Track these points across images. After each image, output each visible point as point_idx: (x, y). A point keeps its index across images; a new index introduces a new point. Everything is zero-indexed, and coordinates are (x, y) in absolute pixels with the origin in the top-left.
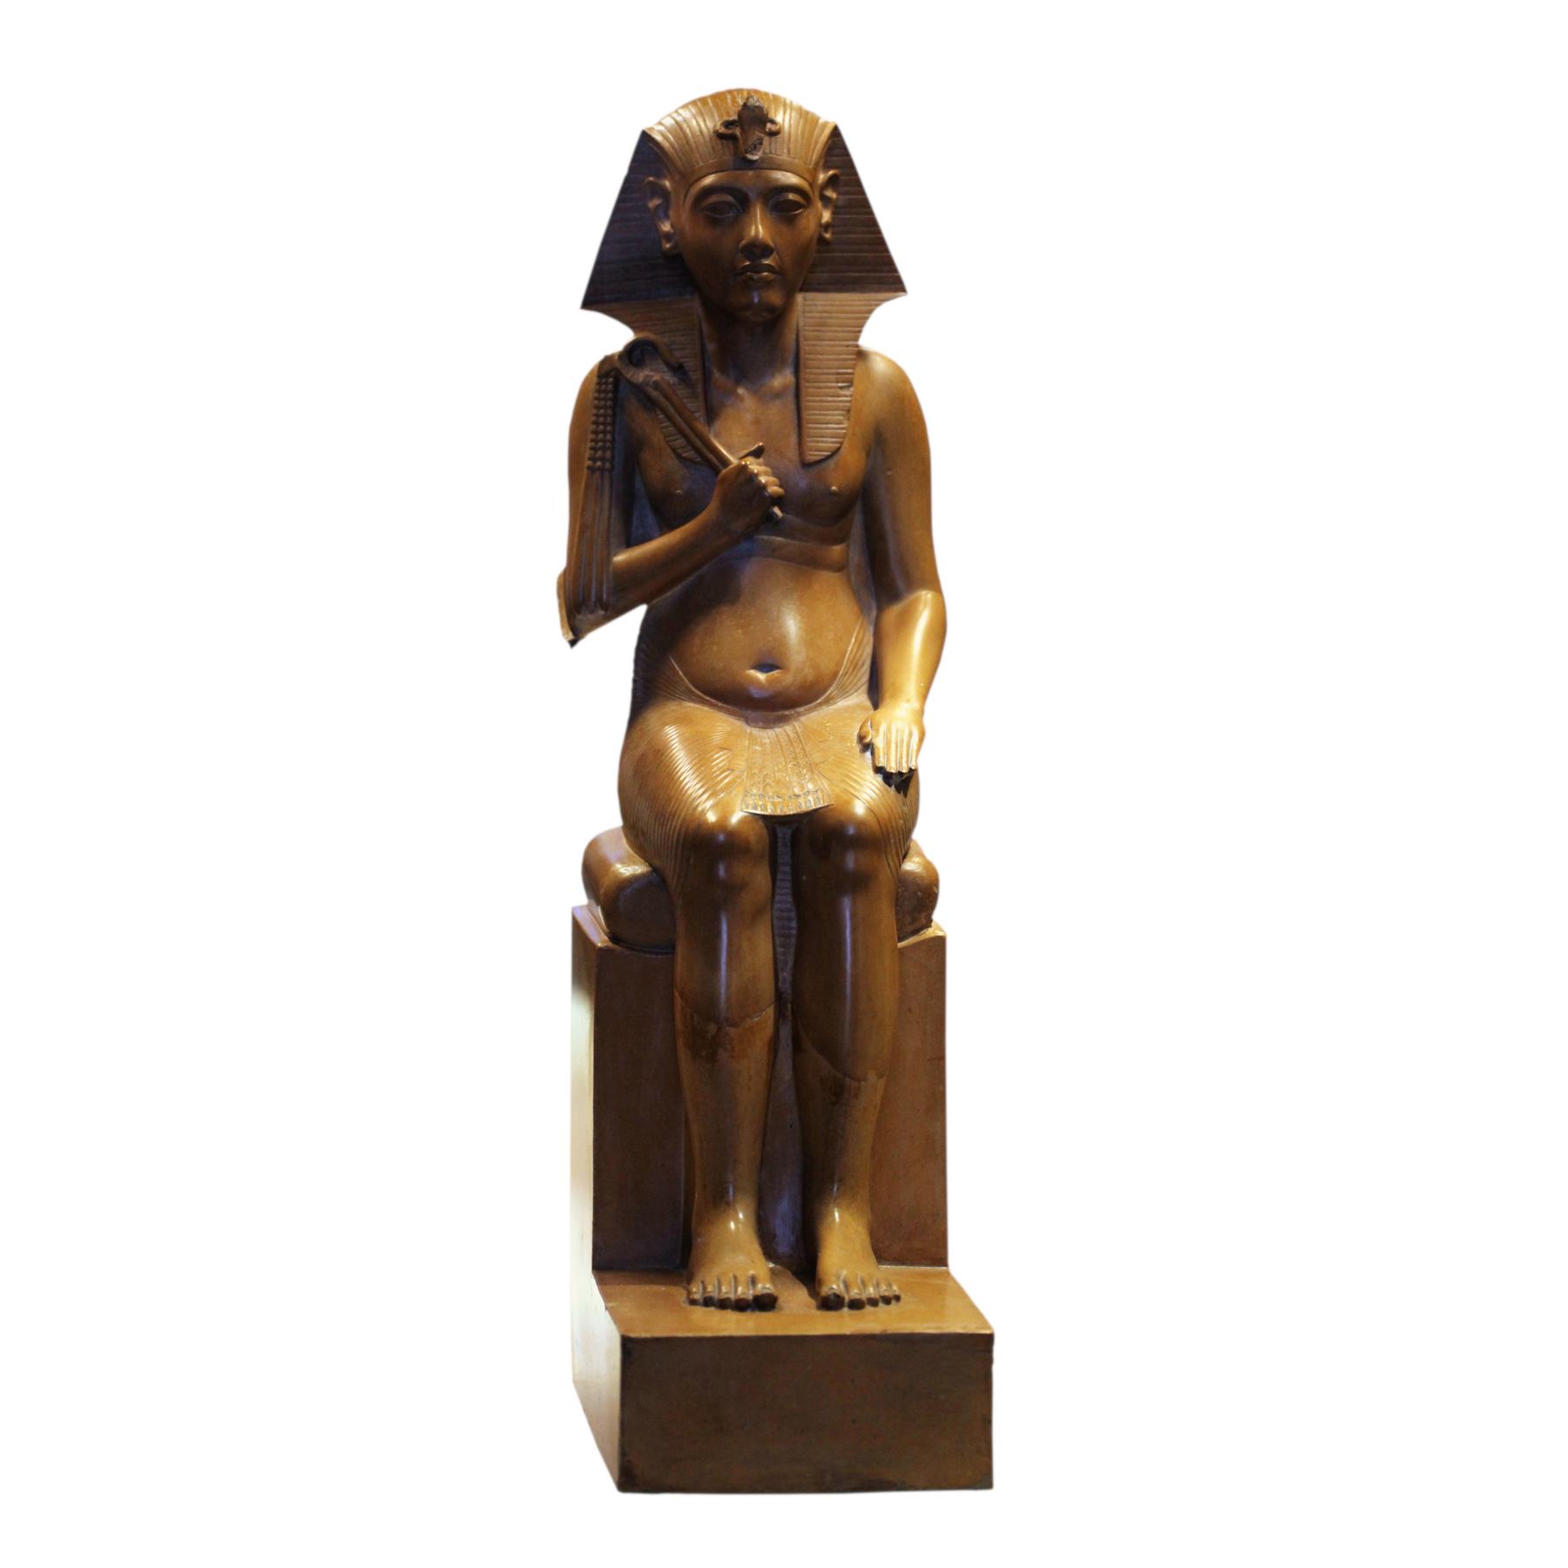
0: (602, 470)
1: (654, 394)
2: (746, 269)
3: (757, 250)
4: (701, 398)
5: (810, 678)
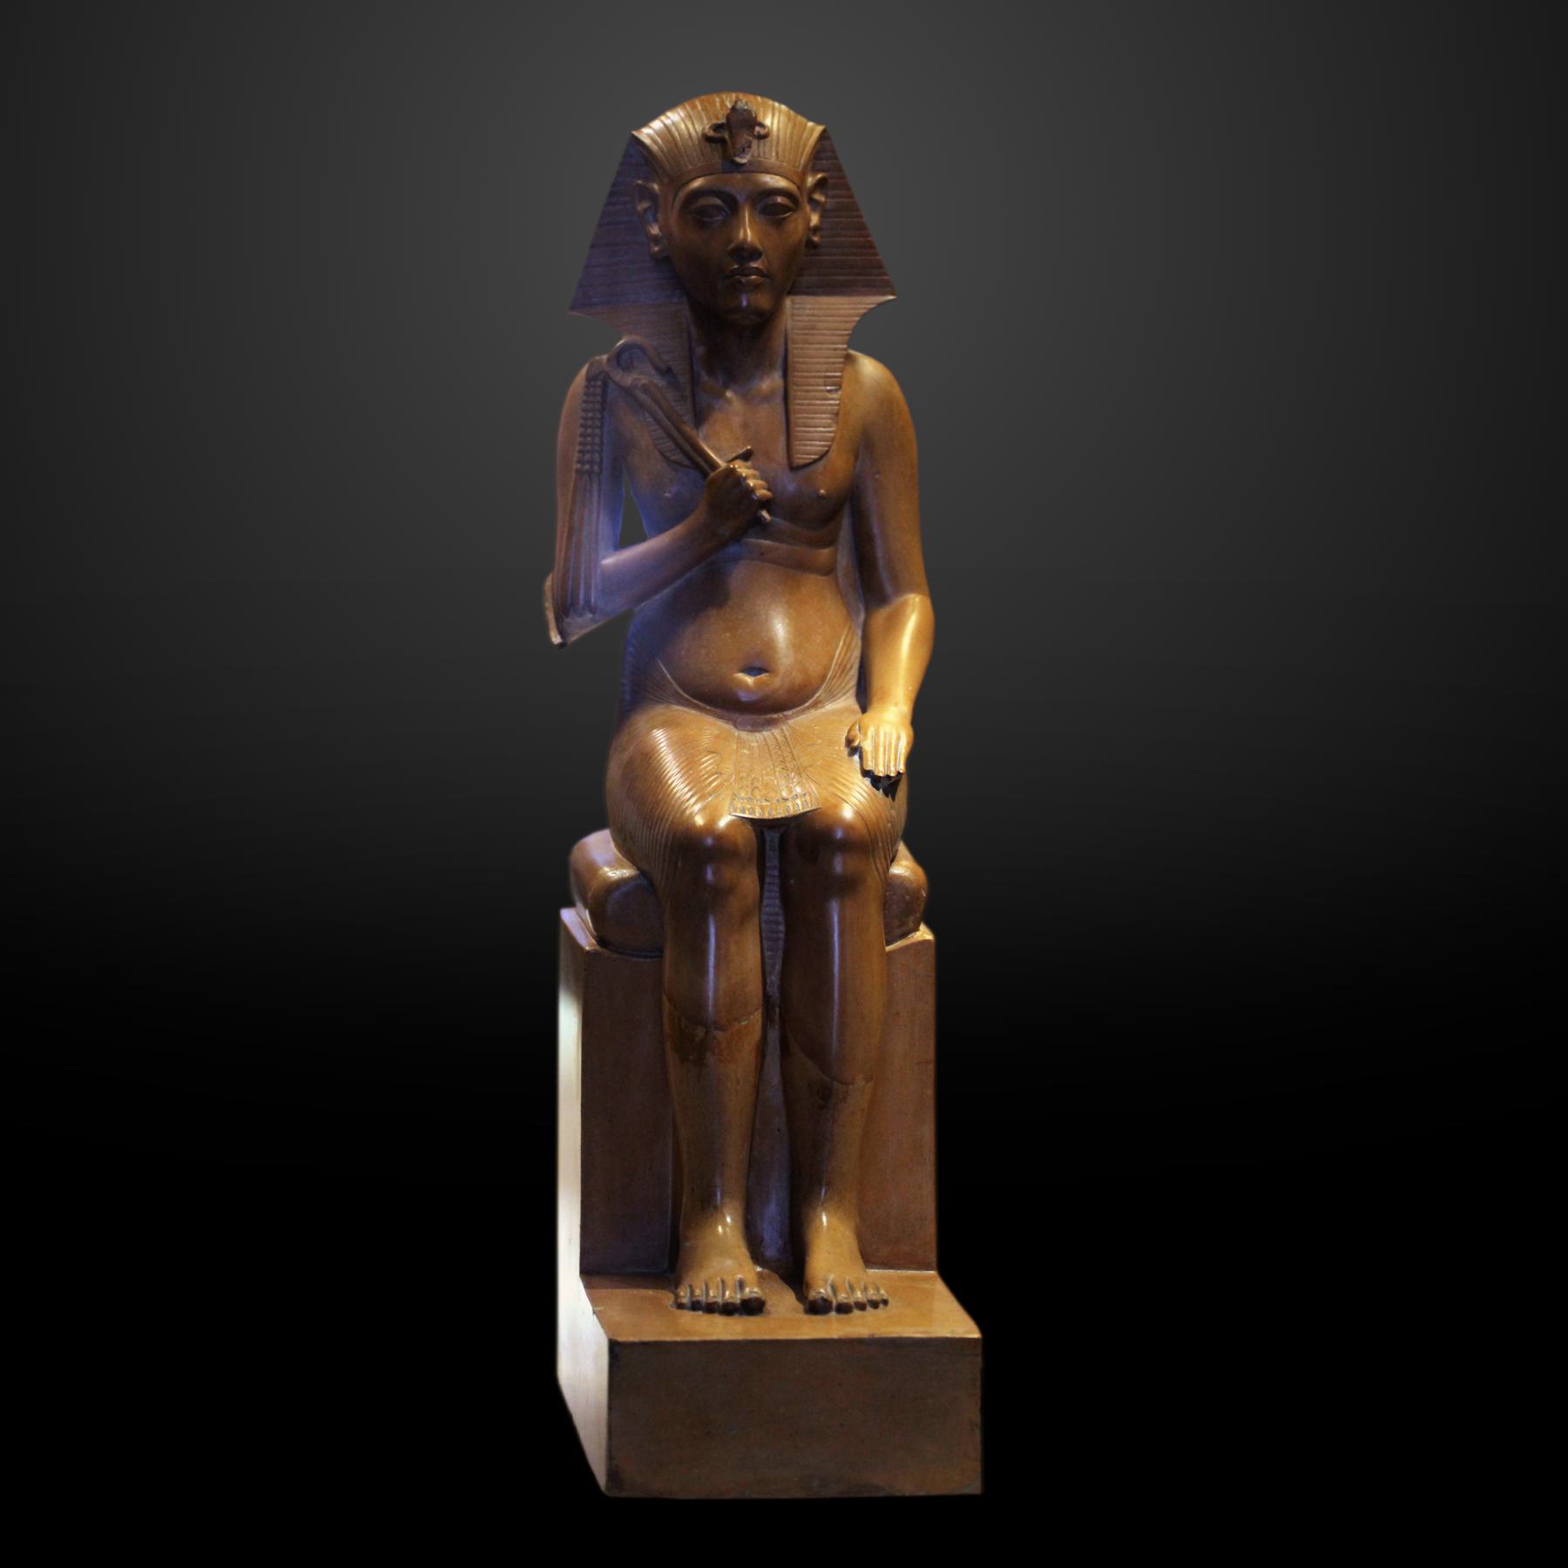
0: (590, 473)
1: (643, 397)
2: (734, 272)
3: (746, 253)
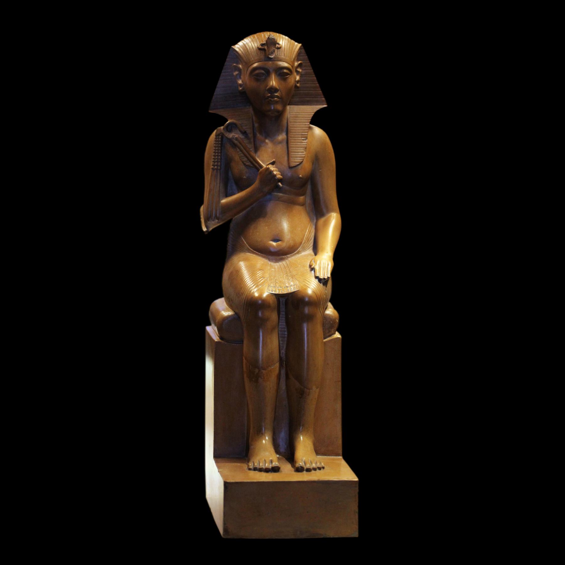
0: (217, 169)
1: (236, 142)
2: (269, 97)
3: (273, 90)
4: (253, 144)
5: (292, 244)
